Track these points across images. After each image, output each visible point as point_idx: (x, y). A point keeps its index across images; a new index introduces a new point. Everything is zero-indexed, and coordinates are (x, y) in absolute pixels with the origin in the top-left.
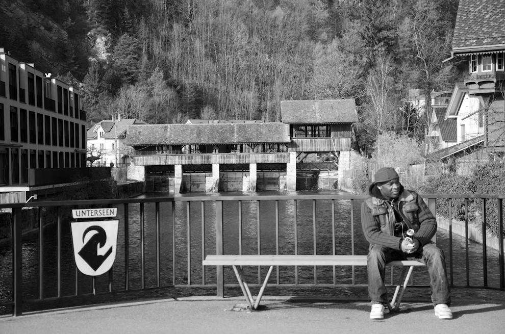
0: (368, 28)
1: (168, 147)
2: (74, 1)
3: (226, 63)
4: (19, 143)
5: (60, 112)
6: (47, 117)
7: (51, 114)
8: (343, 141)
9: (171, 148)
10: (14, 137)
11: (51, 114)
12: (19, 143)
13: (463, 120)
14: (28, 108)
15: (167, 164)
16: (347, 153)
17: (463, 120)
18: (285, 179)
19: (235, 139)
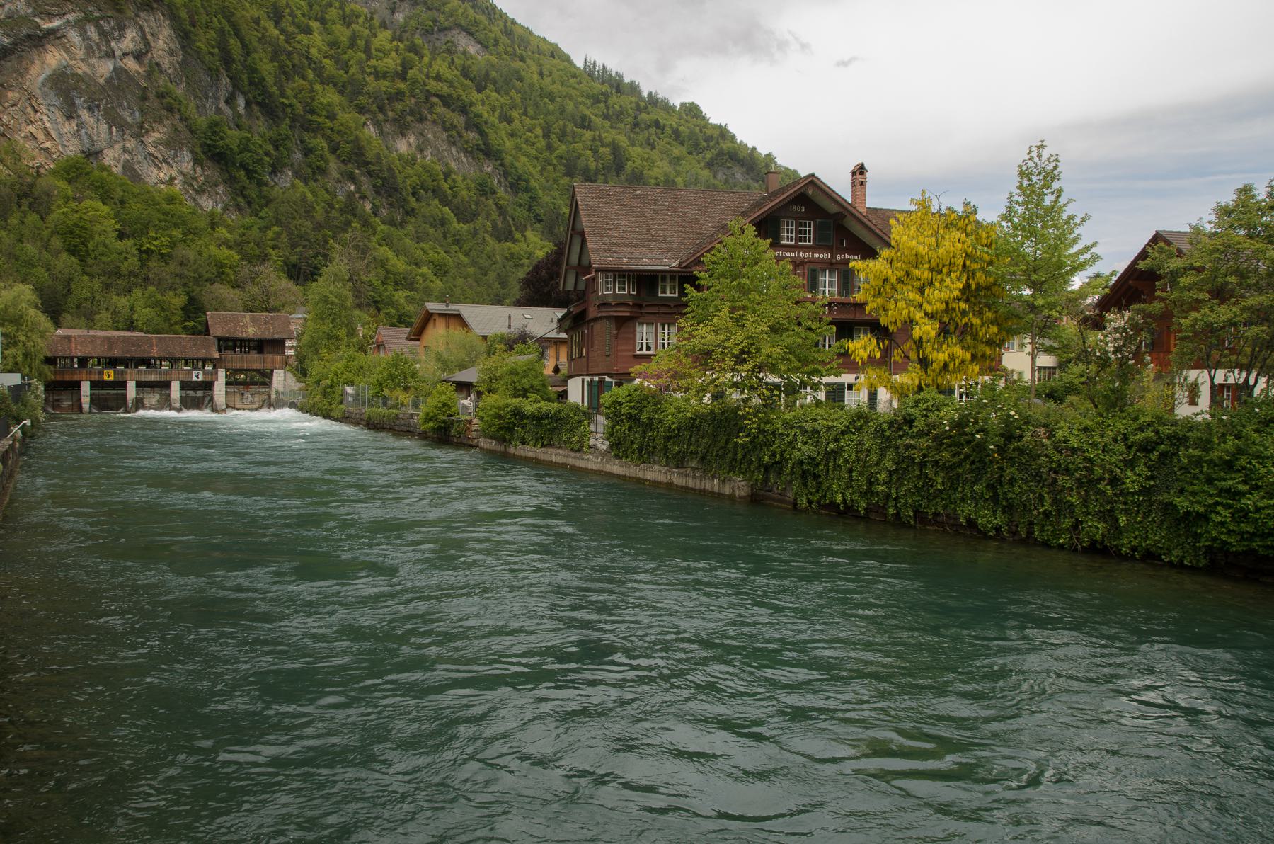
16: (281, 371)
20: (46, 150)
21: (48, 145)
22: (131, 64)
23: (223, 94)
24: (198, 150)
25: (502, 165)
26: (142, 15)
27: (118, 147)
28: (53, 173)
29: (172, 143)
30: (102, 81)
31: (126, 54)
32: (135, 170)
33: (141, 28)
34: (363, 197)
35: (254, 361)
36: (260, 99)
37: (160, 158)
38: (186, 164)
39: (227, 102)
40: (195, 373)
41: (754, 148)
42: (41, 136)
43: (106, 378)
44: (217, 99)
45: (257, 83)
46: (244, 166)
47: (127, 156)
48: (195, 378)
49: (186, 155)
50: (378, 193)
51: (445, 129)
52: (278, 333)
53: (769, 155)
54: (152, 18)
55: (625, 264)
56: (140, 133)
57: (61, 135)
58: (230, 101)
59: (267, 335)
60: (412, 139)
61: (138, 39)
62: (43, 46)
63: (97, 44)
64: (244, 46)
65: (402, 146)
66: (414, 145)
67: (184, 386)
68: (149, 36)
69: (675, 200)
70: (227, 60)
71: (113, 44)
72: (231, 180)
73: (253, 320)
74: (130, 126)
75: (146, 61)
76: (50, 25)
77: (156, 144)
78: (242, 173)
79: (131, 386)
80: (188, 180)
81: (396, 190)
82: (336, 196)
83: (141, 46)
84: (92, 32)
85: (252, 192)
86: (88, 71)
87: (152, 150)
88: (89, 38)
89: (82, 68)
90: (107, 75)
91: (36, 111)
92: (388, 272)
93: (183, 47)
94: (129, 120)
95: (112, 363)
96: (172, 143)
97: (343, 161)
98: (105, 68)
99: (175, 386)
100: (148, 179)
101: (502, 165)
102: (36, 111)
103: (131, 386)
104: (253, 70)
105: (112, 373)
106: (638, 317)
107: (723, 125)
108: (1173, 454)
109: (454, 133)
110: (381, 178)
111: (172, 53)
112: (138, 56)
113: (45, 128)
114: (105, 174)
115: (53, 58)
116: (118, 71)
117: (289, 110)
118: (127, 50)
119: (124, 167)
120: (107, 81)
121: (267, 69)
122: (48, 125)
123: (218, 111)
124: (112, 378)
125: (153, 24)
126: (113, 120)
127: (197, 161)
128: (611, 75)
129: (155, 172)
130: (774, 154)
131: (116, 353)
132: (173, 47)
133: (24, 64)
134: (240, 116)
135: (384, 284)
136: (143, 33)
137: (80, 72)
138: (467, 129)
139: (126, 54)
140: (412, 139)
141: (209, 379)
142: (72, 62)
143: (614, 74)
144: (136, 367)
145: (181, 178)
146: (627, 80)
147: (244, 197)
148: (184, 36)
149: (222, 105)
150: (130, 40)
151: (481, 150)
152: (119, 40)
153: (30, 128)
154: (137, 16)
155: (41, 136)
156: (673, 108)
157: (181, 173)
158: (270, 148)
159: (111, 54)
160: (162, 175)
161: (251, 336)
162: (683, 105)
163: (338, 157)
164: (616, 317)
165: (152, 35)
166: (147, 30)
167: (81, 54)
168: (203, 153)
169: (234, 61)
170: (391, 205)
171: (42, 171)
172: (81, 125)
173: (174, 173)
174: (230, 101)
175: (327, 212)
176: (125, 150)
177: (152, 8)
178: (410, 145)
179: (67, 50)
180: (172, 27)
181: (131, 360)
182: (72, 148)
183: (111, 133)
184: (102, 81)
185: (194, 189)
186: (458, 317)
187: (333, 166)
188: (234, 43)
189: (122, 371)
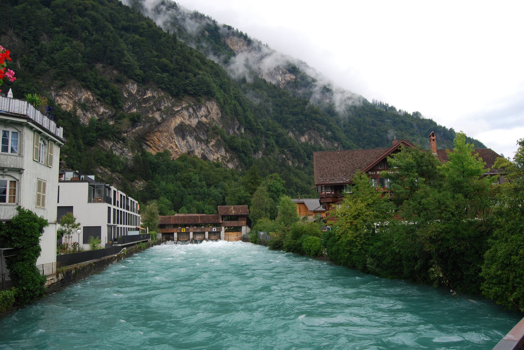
0: (310, 183)
1: (171, 225)
2: (1, 56)
3: (23, 109)
4: (116, 224)
5: (131, 211)
6: (126, 213)
7: (128, 212)
8: (243, 222)
9: (172, 226)
10: (114, 222)
11: (128, 212)
12: (116, 224)
13: (59, 186)
14: (120, 209)
15: (96, 249)
16: (245, 227)
17: (59, 186)
18: (266, 216)
19: (199, 222)
20: (176, 151)
21: (177, 150)
22: (204, 119)
23: (236, 127)
24: (227, 147)
25: (341, 143)
26: (207, 102)
27: (200, 148)
28: (178, 159)
29: (218, 146)
30: (194, 126)
31: (202, 116)
32: (206, 156)
33: (207, 107)
34: (288, 159)
35: (234, 223)
36: (249, 127)
37: (214, 151)
38: (223, 152)
39: (237, 129)
40: (213, 228)
41: (444, 127)
42: (174, 147)
43: (182, 231)
44: (234, 128)
45: (249, 122)
46: (243, 152)
47: (203, 151)
48: (213, 230)
49: (223, 150)
50: (294, 158)
51: (318, 132)
52: (243, 213)
53: (451, 129)
54: (210, 103)
55: (328, 182)
56: (207, 142)
57: (181, 146)
58: (239, 129)
59: (239, 214)
60: (306, 137)
61: (206, 111)
62: (175, 117)
63: (193, 114)
64: (243, 109)
65: (303, 139)
66: (307, 139)
67: (210, 233)
68: (209, 109)
69: (353, 155)
70: (236, 114)
71: (198, 113)
72: (239, 157)
73: (234, 208)
74: (203, 141)
75: (209, 118)
76: (177, 110)
77: (212, 146)
78: (243, 154)
79: (191, 234)
80: (224, 158)
81: (301, 156)
82: (278, 160)
83: (207, 113)
84: (191, 110)
85: (247, 160)
86: (190, 123)
87: (211, 148)
88: (190, 112)
89: (187, 122)
90: (196, 124)
91: (173, 139)
92: (298, 187)
93: (221, 112)
94: (203, 139)
95: (185, 226)
96: (218, 146)
97: (281, 147)
98: (194, 122)
99: (207, 233)
100: (210, 159)
101: (341, 143)
102: (173, 139)
103: (191, 234)
104: (246, 117)
105: (184, 229)
106: (336, 202)
107: (431, 119)
108: (115, 240)
109: (322, 133)
110: (295, 152)
111: (218, 114)
112: (206, 117)
113: (176, 144)
114: (195, 159)
115: (177, 121)
116: (199, 122)
117: (260, 130)
118: (202, 115)
119: (202, 155)
120: (196, 126)
121: (251, 116)
122: (177, 143)
123: (234, 133)
124: (184, 231)
125: (211, 105)
126: (198, 139)
127: (226, 151)
128: (383, 104)
129: (213, 156)
130: (453, 128)
131: (186, 222)
132: (217, 112)
133: (169, 124)
134: (242, 134)
135: (296, 192)
136: (208, 109)
137: (187, 124)
138: (327, 131)
139: (202, 116)
140: (306, 137)
141: (219, 230)
142: (184, 121)
143: (384, 104)
144: (193, 227)
145: (221, 157)
146: (390, 106)
147: (244, 163)
148: (222, 108)
149: (236, 130)
150: (203, 111)
151: (333, 138)
152: (199, 112)
153: (171, 145)
154: (206, 103)
155: (174, 147)
156: (409, 115)
157: (221, 156)
158: (254, 145)
159: (197, 117)
160: (215, 157)
161: (233, 214)
162: (414, 113)
163: (279, 145)
164: (327, 202)
165: (211, 109)
166: (209, 107)
167: (187, 118)
168: (229, 148)
169: (239, 115)
170: (299, 162)
171: (175, 159)
172: (187, 142)
173: (219, 156)
174: (239, 129)
175: (274, 166)
176: (202, 149)
177: (211, 100)
178: (306, 139)
179: (183, 118)
180: (217, 105)
181: (191, 224)
182: (185, 150)
183: (197, 144)
184: (194, 126)
185: (226, 161)
186: (303, 203)
187: (277, 150)
188: (239, 108)
189: (188, 229)
